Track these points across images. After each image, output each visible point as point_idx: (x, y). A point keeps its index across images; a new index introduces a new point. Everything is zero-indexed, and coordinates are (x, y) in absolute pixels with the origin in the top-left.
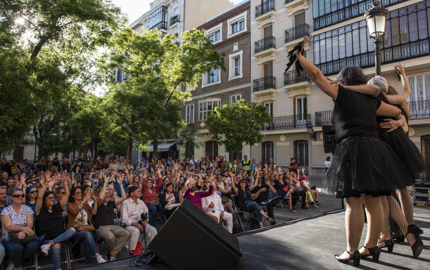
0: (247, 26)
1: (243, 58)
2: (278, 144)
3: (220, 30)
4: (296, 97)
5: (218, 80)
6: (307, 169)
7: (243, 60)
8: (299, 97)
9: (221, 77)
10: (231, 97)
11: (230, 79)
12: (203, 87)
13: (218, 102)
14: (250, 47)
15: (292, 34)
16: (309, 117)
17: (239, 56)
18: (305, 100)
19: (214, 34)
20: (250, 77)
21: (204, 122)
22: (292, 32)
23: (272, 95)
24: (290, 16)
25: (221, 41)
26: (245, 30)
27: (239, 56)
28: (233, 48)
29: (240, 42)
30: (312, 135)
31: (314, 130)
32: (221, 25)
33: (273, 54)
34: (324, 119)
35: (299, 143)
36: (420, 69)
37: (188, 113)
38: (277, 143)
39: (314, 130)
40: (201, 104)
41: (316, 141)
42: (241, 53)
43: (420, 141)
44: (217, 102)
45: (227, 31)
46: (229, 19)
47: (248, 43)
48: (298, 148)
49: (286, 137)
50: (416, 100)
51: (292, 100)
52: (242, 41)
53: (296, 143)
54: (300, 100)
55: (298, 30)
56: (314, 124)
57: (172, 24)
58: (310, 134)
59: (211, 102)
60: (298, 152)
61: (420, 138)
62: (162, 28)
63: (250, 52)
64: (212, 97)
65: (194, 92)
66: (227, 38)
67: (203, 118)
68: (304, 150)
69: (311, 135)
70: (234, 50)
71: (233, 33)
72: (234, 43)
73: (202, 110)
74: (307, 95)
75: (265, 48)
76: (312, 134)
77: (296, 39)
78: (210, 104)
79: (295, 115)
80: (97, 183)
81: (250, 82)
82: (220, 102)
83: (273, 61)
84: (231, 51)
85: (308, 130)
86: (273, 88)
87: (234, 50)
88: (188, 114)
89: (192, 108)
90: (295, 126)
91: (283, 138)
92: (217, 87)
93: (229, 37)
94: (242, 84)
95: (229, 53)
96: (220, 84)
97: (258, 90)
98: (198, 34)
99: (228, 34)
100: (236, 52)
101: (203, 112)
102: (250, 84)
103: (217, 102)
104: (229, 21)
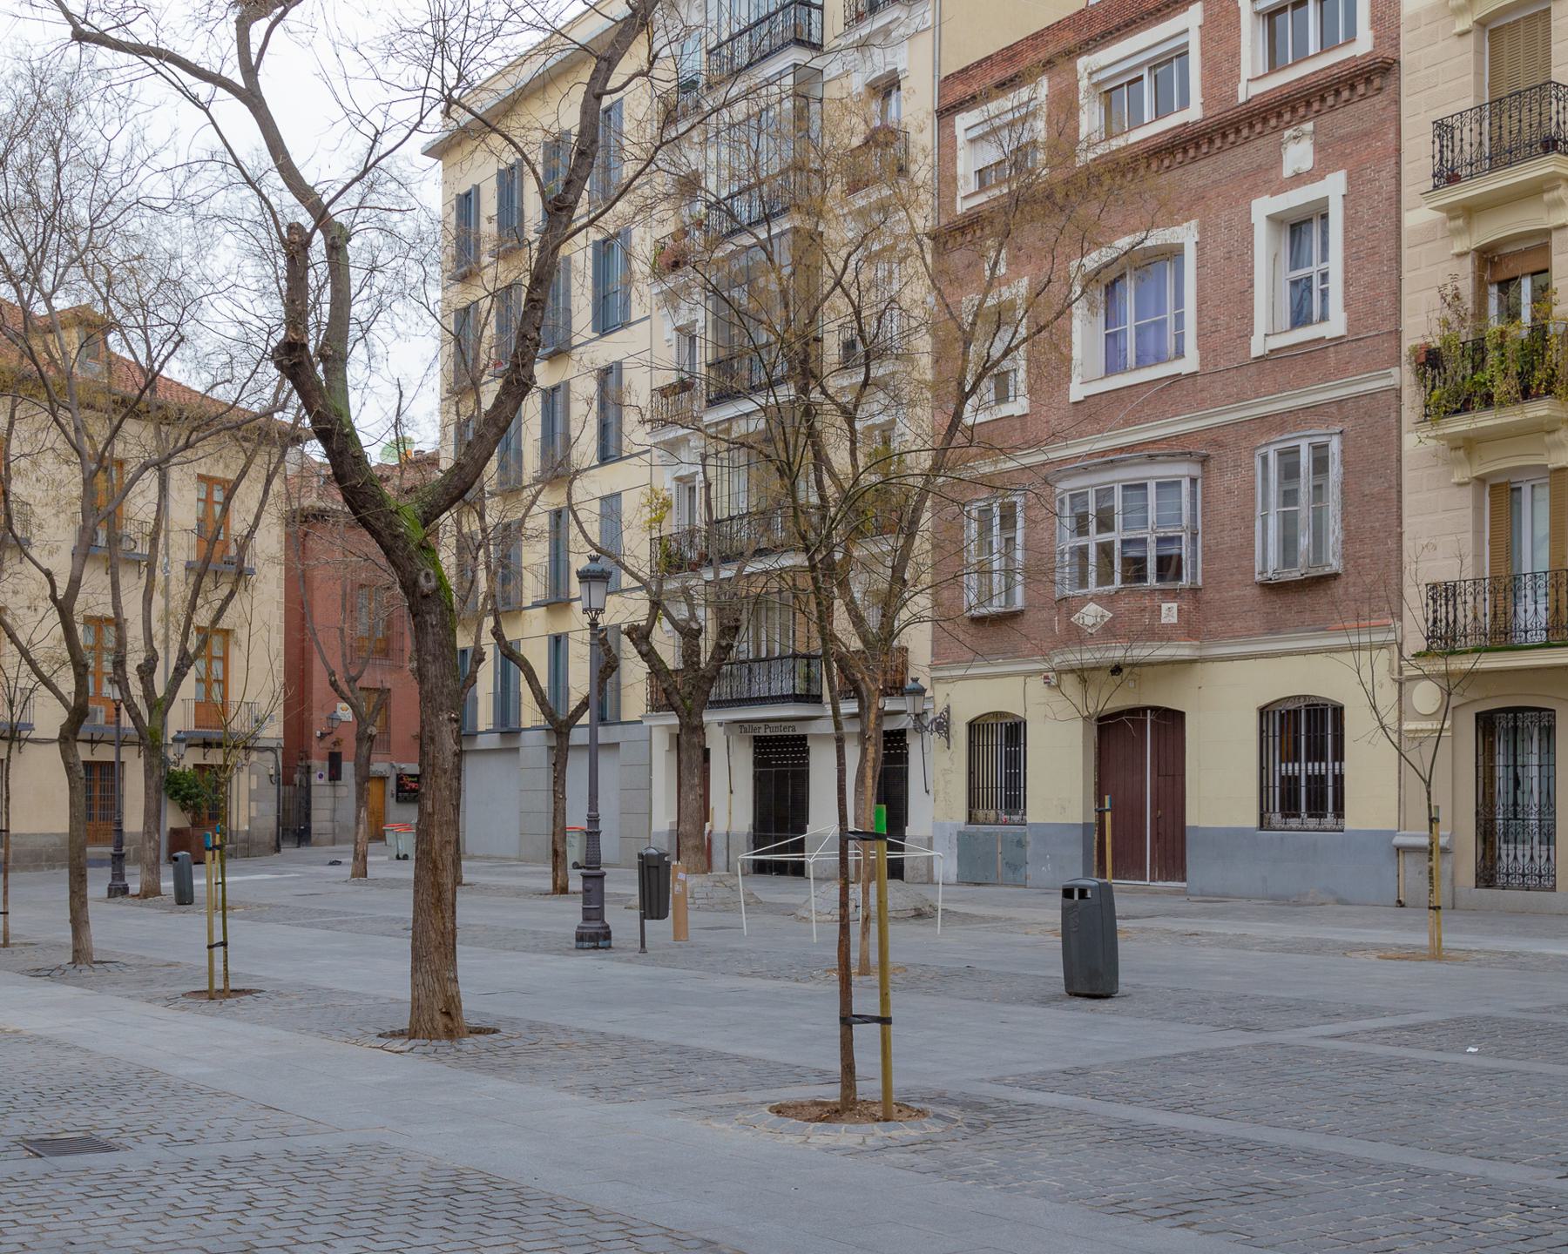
0: (1376, 21)
1: (1350, 222)
3: (1187, 44)
6: (1548, 859)
7: (1346, 231)
9: (1201, 335)
11: (1258, 347)
13: (1186, 484)
14: (1398, 150)
15: (1475, 140)
17: (1324, 201)
19: (1145, 72)
20: (1397, 334)
21: (1097, 599)
22: (1475, 126)
24: (1462, 34)
25: (1194, 112)
26: (1364, 44)
27: (1324, 201)
28: (1279, 161)
29: (1326, 119)
32: (1042, 89)
33: (1557, 187)
35: (1503, 722)
40: (1078, 497)
42: (1334, 187)
45: (1235, 54)
46: (1088, 52)
47: (1383, 122)
48: (1500, 748)
52: (1339, 115)
53: (1486, 723)
55: (1505, 117)
57: (860, 17)
59: (1144, 486)
60: (1500, 772)
62: (799, 42)
63: (1399, 184)
66: (1235, 96)
67: (1092, 578)
68: (1535, 760)
70: (1287, 172)
71: (1274, 66)
72: (1288, 125)
73: (1086, 533)
75: (1500, 156)
77: (1491, 169)
80: (860, 974)
81: (1397, 362)
82: (1193, 481)
83: (1555, 236)
84: (1267, 178)
87: (1287, 172)
89: (1320, 464)
93: (1246, 91)
94: (1341, 371)
95: (1255, 191)
96: (1338, 341)
99: (1246, 72)
100: (1299, 179)
101: (1093, 539)
102: (1395, 371)
104: (1084, 63)
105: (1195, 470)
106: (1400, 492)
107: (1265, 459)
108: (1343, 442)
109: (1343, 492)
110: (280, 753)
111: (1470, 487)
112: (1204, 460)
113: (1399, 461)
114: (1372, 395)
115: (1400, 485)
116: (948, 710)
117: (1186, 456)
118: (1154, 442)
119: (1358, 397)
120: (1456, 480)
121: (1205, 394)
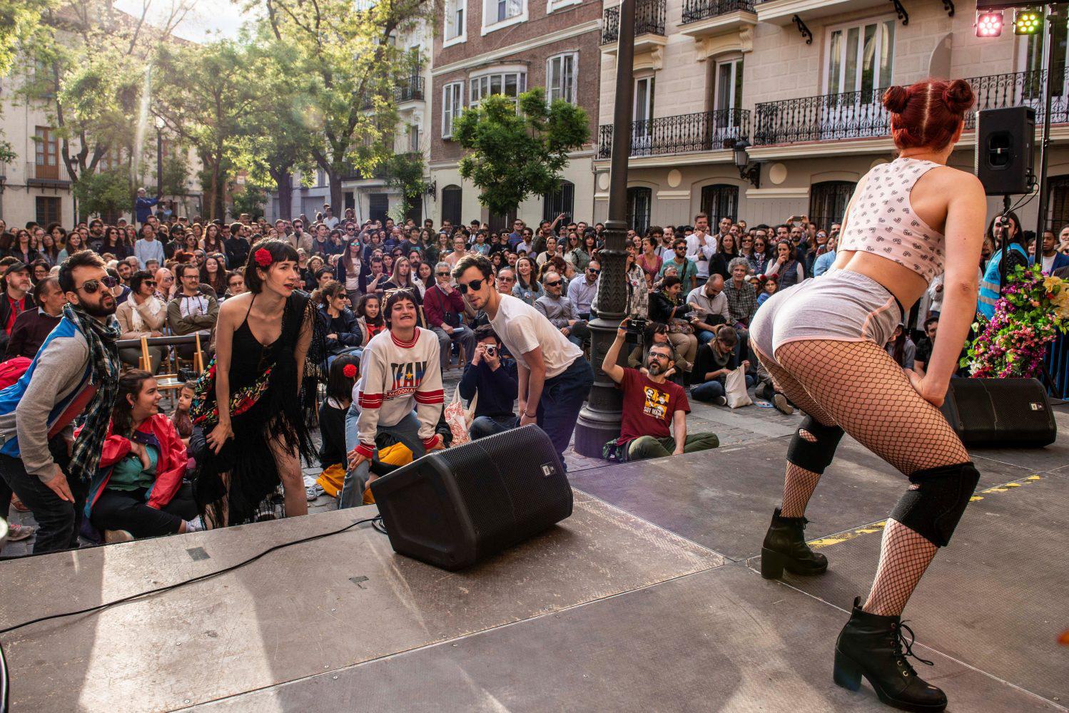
2: (661, 194)
4: (717, 60)
5: (521, 14)
8: (725, 61)
10: (550, 60)
12: (484, 31)
13: (519, 76)
16: (745, 119)
18: (740, 67)
23: (653, 54)
30: (746, 171)
31: (751, 157)
34: (789, 124)
36: (834, 16)
37: (448, 107)
38: (660, 193)
39: (751, 157)
40: (475, 81)
41: (758, 187)
43: (808, 196)
44: (515, 76)
49: (683, 177)
50: (841, 90)
51: (704, 67)
53: (708, 193)
54: (726, 68)
56: (751, 140)
58: (738, 167)
59: (500, 77)
61: (806, 190)
64: (501, 61)
65: (463, 46)
69: (742, 171)
73: (477, 99)
74: (744, 54)
76: (745, 167)
78: (496, 80)
79: (709, 114)
82: (523, 75)
85: (734, 157)
86: (656, 33)
88: (446, 109)
90: (708, 144)
91: (674, 180)
92: (517, 32)
96: (525, 23)
97: (699, 19)
98: (113, 107)
102: (599, 21)
103: (515, 76)
105: (524, 69)
106: (599, 81)
107: (448, 89)
108: (579, 56)
109: (578, 81)
110: (201, 197)
111: (705, 63)
112: (529, 64)
113: (600, 65)
114: (590, 33)
115: (599, 77)
116: (435, 183)
117: (519, 62)
118: (511, 56)
119: (585, 34)
120: (699, 58)
121: (530, 32)
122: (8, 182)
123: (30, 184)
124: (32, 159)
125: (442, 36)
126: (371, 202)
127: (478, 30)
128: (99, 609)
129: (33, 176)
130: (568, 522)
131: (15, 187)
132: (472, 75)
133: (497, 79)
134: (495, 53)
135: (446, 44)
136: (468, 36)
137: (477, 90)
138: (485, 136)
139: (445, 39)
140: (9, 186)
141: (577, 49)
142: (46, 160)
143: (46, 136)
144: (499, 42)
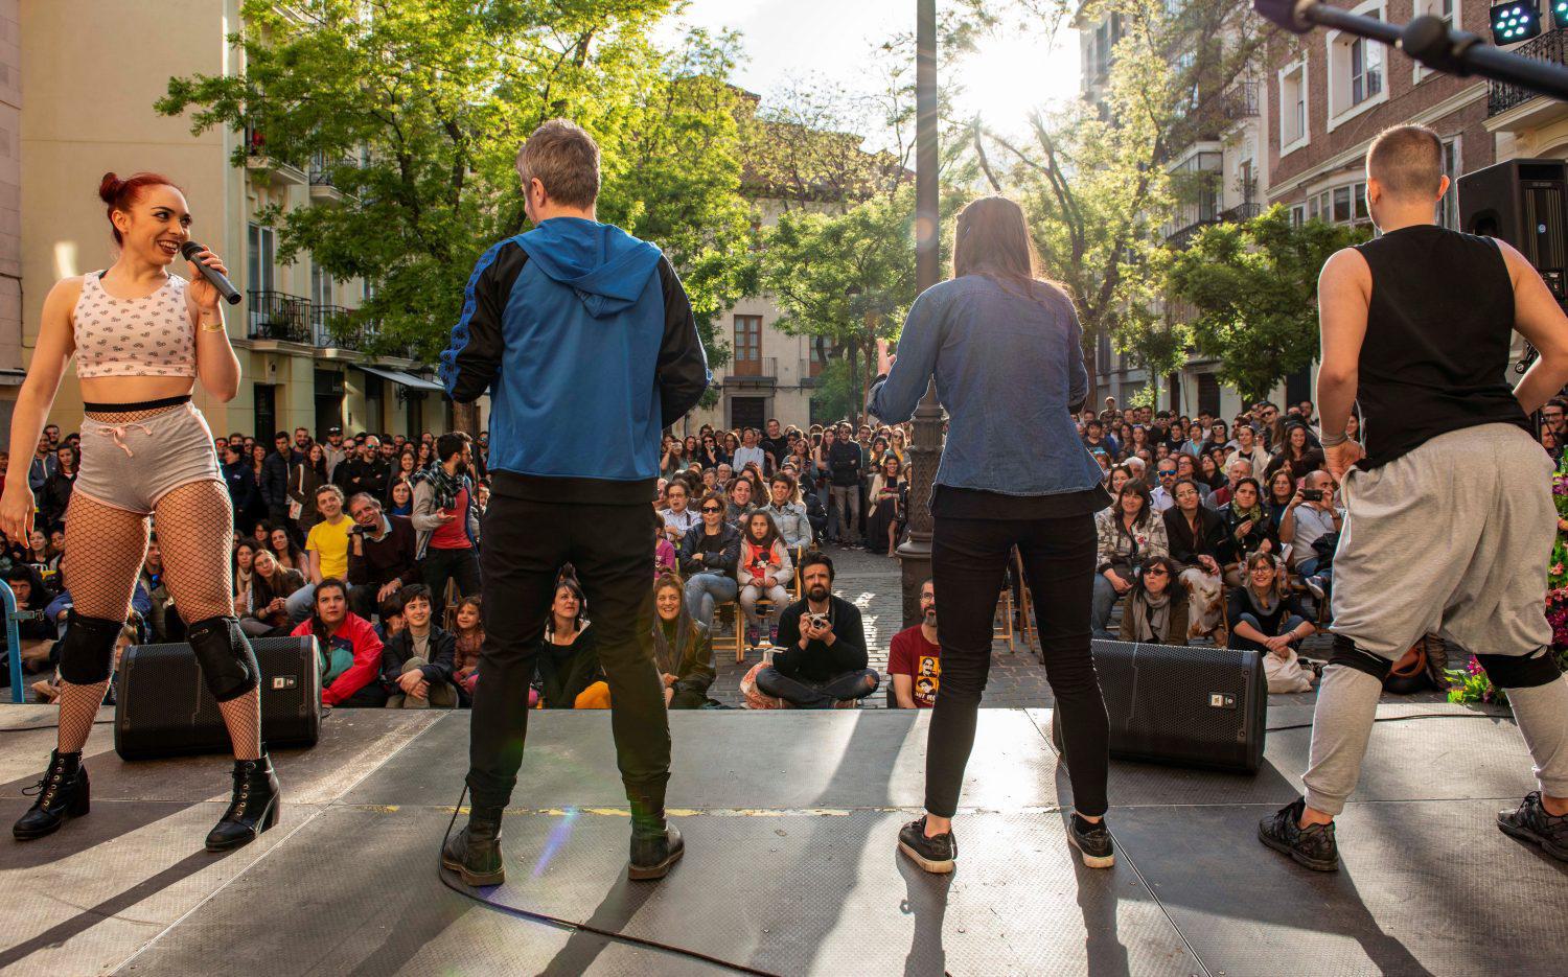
12: (1331, 125)
92: (1376, 117)
96: (1386, 103)
113: (1494, 150)
122: (780, 383)
123: (804, 384)
124: (806, 356)
125: (1279, 141)
126: (1200, 385)
127: (1324, 125)
128: (581, 928)
129: (807, 376)
130: (204, 818)
131: (787, 389)
132: (1310, 191)
133: (1344, 194)
134: (1345, 156)
135: (1284, 153)
136: (1312, 136)
137: (1347, 204)
138: (1199, 286)
139: (1282, 145)
140: (781, 388)
141: (1459, 131)
142: (747, 354)
143: (747, 326)
144: (1351, 137)
